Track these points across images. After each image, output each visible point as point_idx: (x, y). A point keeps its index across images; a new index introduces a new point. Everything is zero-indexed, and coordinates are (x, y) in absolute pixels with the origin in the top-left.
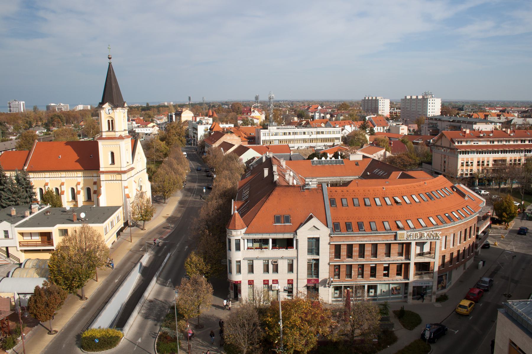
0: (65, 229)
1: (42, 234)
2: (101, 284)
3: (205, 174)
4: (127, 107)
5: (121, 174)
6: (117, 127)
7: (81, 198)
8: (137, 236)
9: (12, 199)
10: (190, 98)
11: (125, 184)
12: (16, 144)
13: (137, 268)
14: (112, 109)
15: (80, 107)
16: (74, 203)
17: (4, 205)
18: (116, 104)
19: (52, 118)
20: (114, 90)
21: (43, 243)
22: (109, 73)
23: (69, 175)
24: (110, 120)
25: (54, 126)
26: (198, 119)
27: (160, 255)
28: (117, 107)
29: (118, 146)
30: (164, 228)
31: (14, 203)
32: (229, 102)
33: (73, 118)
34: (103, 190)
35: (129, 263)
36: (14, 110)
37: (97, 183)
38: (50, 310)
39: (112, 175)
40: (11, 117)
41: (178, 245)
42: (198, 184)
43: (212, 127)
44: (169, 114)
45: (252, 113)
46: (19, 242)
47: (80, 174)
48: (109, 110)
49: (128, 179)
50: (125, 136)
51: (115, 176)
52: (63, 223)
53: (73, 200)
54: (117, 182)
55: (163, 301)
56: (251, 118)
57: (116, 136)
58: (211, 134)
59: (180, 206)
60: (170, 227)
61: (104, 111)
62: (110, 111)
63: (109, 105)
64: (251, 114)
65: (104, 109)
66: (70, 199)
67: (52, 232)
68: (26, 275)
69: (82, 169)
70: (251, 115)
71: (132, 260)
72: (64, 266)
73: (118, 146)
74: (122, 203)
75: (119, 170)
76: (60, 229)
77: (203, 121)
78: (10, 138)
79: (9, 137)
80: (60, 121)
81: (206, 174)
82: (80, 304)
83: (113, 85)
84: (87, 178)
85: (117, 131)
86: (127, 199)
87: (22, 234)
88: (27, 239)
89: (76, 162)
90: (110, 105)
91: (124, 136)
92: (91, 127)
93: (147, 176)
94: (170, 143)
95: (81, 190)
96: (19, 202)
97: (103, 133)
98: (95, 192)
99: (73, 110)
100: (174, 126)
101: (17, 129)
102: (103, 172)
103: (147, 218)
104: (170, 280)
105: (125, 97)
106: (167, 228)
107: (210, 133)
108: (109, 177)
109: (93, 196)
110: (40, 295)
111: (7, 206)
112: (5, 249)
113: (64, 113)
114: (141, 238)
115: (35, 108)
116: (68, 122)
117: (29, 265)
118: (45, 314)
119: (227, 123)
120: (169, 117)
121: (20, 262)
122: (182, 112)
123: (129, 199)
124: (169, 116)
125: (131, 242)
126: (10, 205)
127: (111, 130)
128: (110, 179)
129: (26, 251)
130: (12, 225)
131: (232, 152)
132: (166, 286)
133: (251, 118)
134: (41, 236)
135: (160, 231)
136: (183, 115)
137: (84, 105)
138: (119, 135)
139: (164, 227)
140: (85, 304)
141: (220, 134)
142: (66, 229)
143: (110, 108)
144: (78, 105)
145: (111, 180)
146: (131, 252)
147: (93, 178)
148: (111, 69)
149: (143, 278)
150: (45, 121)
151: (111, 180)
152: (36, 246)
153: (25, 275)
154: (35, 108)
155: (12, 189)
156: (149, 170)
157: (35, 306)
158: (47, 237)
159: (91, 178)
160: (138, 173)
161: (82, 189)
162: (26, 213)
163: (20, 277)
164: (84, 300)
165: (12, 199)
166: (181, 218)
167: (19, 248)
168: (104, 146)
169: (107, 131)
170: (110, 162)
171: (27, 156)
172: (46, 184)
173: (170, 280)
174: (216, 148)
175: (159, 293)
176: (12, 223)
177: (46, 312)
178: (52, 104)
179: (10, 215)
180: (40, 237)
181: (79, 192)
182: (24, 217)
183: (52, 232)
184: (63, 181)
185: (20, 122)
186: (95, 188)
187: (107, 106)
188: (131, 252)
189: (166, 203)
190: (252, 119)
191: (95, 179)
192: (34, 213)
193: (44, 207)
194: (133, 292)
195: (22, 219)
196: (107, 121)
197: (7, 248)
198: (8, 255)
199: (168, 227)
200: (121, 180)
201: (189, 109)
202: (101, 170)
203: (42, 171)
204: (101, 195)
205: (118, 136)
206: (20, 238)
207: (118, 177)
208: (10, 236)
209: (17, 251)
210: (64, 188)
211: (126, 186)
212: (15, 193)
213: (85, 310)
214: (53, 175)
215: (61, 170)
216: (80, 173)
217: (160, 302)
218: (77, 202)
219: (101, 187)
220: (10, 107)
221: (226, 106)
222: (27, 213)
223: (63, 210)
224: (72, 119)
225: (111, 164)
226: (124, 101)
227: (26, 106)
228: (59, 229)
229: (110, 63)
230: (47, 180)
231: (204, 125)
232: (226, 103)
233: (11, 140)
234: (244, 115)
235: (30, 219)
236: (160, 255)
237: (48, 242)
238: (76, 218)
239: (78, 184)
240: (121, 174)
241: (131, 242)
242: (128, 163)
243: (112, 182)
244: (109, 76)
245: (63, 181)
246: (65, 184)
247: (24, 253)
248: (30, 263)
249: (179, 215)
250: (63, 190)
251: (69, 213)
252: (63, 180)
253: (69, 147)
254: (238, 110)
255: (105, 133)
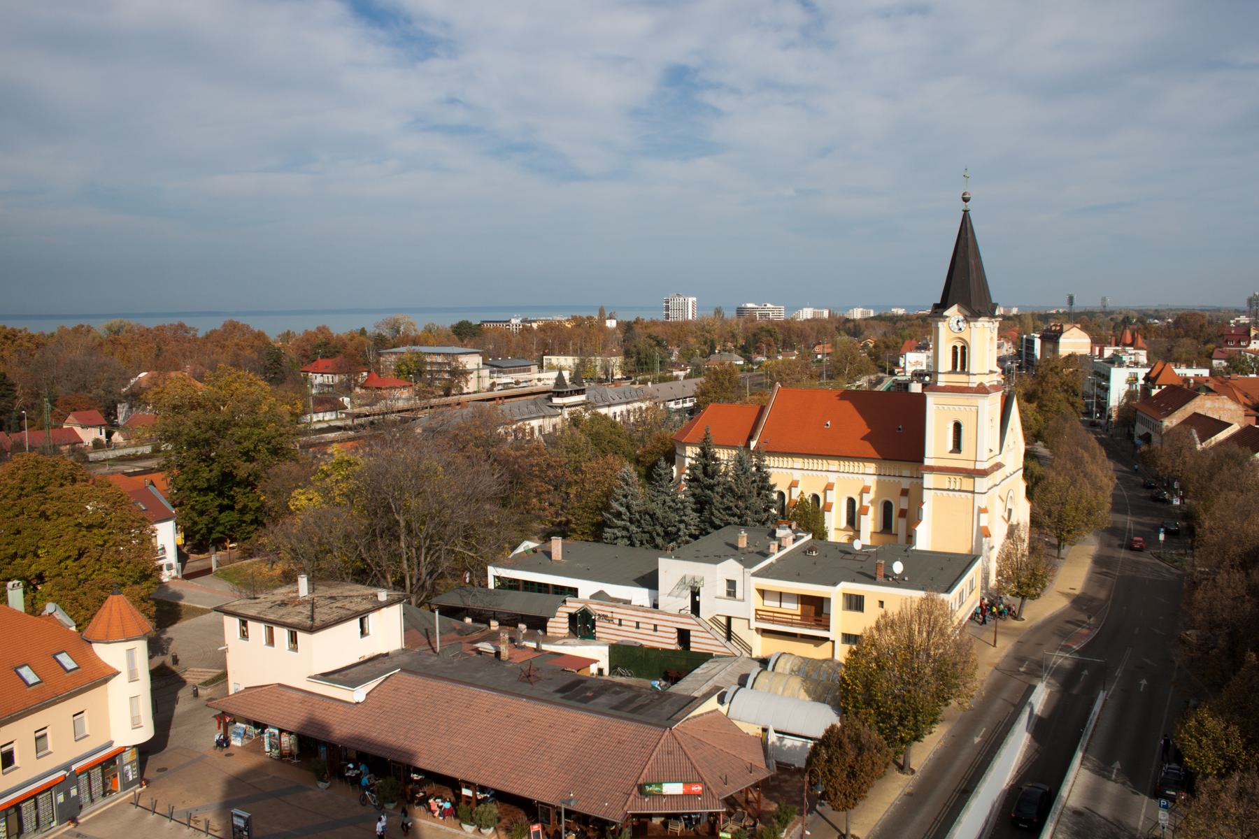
0: (857, 596)
1: (805, 600)
2: (940, 741)
3: (1144, 493)
4: (999, 316)
5: (974, 478)
6: (975, 364)
7: (869, 524)
8: (1009, 633)
9: (735, 510)
10: (1071, 299)
11: (981, 501)
12: (695, 388)
13: (1024, 718)
14: (966, 320)
15: (807, 313)
16: (852, 533)
17: (717, 522)
18: (976, 308)
19: (754, 335)
20: (973, 275)
21: (805, 620)
22: (963, 236)
23: (851, 467)
24: (959, 345)
25: (758, 353)
26: (1108, 352)
27: (1075, 691)
28: (980, 316)
29: (973, 409)
30: (1068, 622)
31: (736, 519)
32: (1163, 311)
33: (798, 337)
34: (927, 509)
35: (998, 704)
36: (675, 316)
37: (914, 496)
38: (859, 788)
39: (952, 477)
40: (675, 330)
41: (1118, 673)
42: (1134, 519)
43: (1153, 375)
44: (1025, 336)
45: (1253, 342)
46: (756, 610)
47: (871, 468)
48: (958, 321)
49: (989, 489)
50: (990, 386)
51: (958, 480)
52: (854, 581)
53: (849, 527)
54: (963, 494)
55: (1110, 818)
56: (1253, 356)
57: (970, 385)
58: (1150, 392)
59: (1098, 570)
60: (1084, 622)
61: (945, 324)
62: (960, 324)
63: (959, 311)
64: (1249, 343)
65: (947, 319)
66: (844, 524)
67: (829, 600)
68: (783, 691)
69: (878, 457)
70: (1248, 345)
71: (1005, 694)
72: (881, 685)
73: (973, 409)
74: (970, 546)
75: (970, 466)
76: (847, 594)
77: (1124, 358)
78: (675, 373)
79: (672, 372)
80: (773, 343)
81: (1149, 495)
82: (900, 783)
83: (972, 262)
84: (887, 479)
85: (975, 373)
86: (984, 539)
87: (763, 593)
88: (772, 604)
89: (863, 439)
90: (962, 310)
91: (988, 385)
92: (846, 359)
93: (1022, 486)
94: (1045, 409)
95: (870, 505)
96: (749, 519)
97: (940, 376)
98: (903, 513)
99: (792, 319)
100: (1056, 367)
101: (687, 356)
102: (932, 469)
103: (1032, 591)
104: (1117, 765)
105: (996, 291)
106: (1079, 624)
107: (1146, 390)
108: (944, 481)
109: (898, 524)
110: (841, 748)
111: (723, 525)
112: (724, 621)
113: (778, 324)
114: (1016, 639)
115: (718, 311)
116: (787, 345)
117: (784, 666)
118: (845, 794)
119: (1189, 366)
120: (1024, 344)
121: (751, 654)
122: (1061, 332)
123: (988, 539)
124: (1024, 341)
125: (995, 646)
126: (730, 524)
127: (959, 369)
128: (947, 487)
129: (765, 632)
130: (746, 570)
131: (1228, 439)
132: (1109, 779)
133: (1253, 356)
134: (801, 604)
135: (1058, 628)
136: (1062, 340)
137: (815, 308)
138: (978, 382)
139: (1067, 619)
140: (911, 784)
141: (1182, 393)
142: (860, 596)
143: (961, 317)
144: (802, 308)
145: (948, 490)
146: (997, 673)
147: (902, 480)
148: (968, 225)
149: (1036, 745)
150: (741, 342)
151: (948, 490)
152: (792, 624)
153: (781, 689)
154: (718, 311)
155: (738, 487)
156: (1028, 474)
157: (826, 770)
158: (816, 609)
159: (897, 479)
160: (1007, 477)
161: (872, 502)
162: (772, 547)
163: (769, 692)
164: (907, 774)
165: (735, 510)
166: (1109, 603)
167: (754, 624)
168: (940, 407)
169: (949, 373)
170: (950, 446)
171: (753, 421)
172: (794, 484)
173: (1117, 765)
174: (1170, 431)
175: (1094, 794)
176: (747, 564)
177: (849, 790)
178: (749, 305)
179: (736, 548)
180: (800, 605)
181: (864, 511)
182: (765, 555)
183: (829, 600)
184: (831, 481)
185: (692, 340)
186: (903, 503)
187: (953, 312)
188: (997, 673)
189: (1062, 559)
190: (1255, 358)
191: (905, 483)
192: (785, 547)
193: (803, 537)
194: (1016, 777)
195: (760, 562)
196: (951, 349)
197: (729, 619)
198: (729, 635)
199: (1080, 621)
200: (973, 492)
201: (1079, 326)
202: (927, 462)
203: (789, 453)
204: (921, 523)
205: (975, 385)
206: (756, 601)
207: (967, 483)
208: (739, 594)
209: (749, 628)
210: (832, 497)
211: (983, 507)
212: (740, 497)
213: (913, 800)
214: (815, 465)
215: (867, 458)
216: (873, 465)
217: (1105, 822)
218: (859, 531)
219: (922, 503)
220: (667, 308)
221: (1156, 321)
222: (774, 546)
223: (843, 549)
224: (794, 338)
225: (951, 452)
226: (994, 301)
227: (699, 307)
228: (844, 594)
229: (966, 212)
230: (797, 475)
231: (1128, 366)
232: (1157, 315)
233: (677, 378)
234: (1229, 346)
235: (778, 560)
236: (1075, 691)
237: (816, 620)
238: (881, 571)
239: (866, 490)
240: (974, 478)
241: (995, 646)
242: (991, 451)
243: (951, 493)
244: (962, 242)
245: (795, 478)
246: (835, 488)
247: (762, 636)
248: (786, 664)
249: (1102, 594)
250: (829, 500)
251: (858, 558)
252: (832, 478)
253: (847, 405)
254: (1201, 331)
255: (943, 376)
